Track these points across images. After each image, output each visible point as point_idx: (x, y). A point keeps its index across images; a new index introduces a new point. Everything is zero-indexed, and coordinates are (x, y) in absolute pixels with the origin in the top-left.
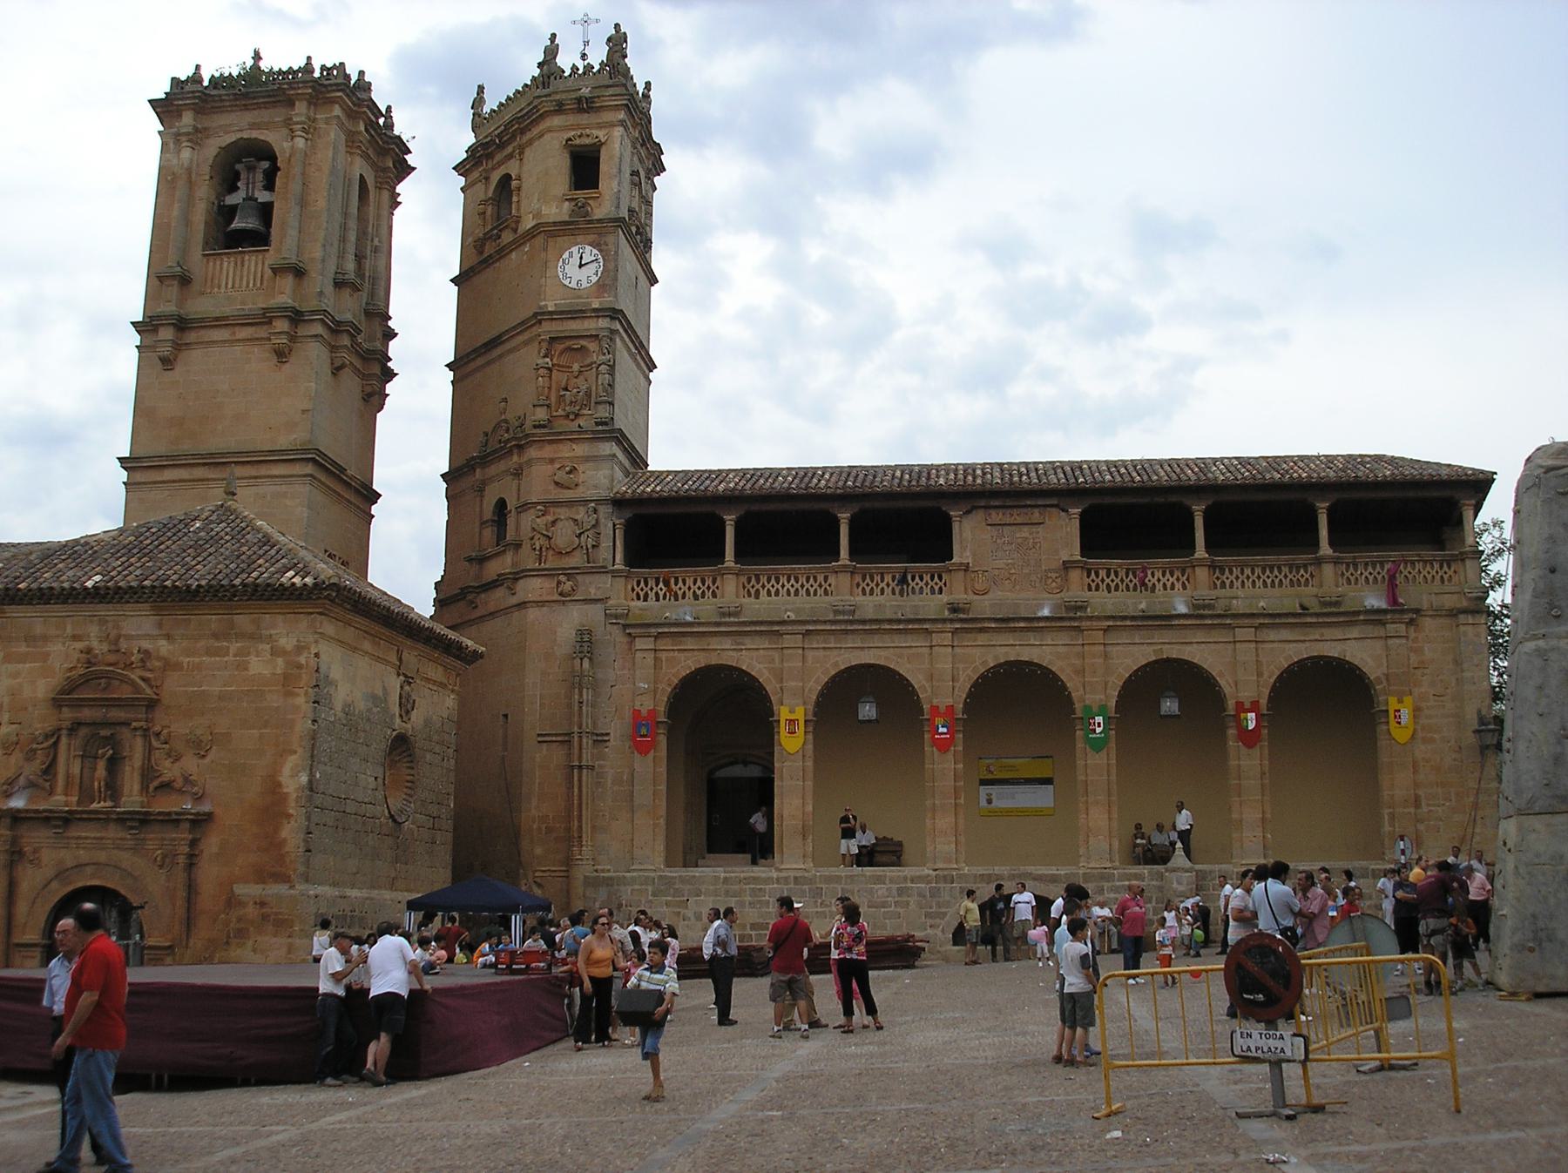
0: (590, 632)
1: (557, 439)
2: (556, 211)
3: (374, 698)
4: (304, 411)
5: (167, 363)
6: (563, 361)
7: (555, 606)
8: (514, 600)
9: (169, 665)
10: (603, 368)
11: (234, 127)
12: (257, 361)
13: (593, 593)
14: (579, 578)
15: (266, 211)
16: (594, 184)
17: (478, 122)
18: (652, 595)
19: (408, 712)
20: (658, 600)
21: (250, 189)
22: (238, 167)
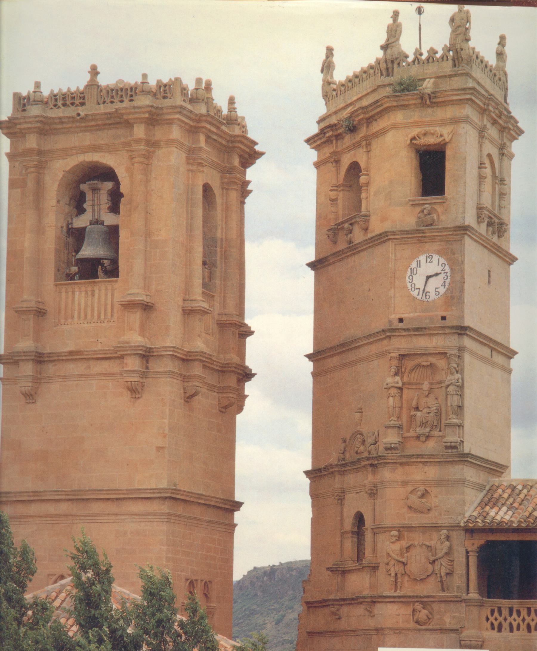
1: (406, 461)
5: (30, 397)
6: (415, 376)
8: (371, 623)
10: (451, 389)
13: (448, 621)
14: (435, 606)
15: (112, 234)
17: (330, 91)
18: (506, 625)
20: (511, 630)
22: (84, 187)
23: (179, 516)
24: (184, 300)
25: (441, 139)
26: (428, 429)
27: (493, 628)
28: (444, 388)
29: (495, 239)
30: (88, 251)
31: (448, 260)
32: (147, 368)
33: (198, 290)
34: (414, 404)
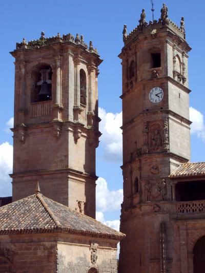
3: (81, 258)
5: (23, 142)
9: (15, 253)
11: (37, 59)
18: (185, 210)
19: (94, 261)
23: (141, 265)
29: (181, 83)
30: (41, 92)
31: (162, 89)
33: (79, 104)
34: (152, 138)
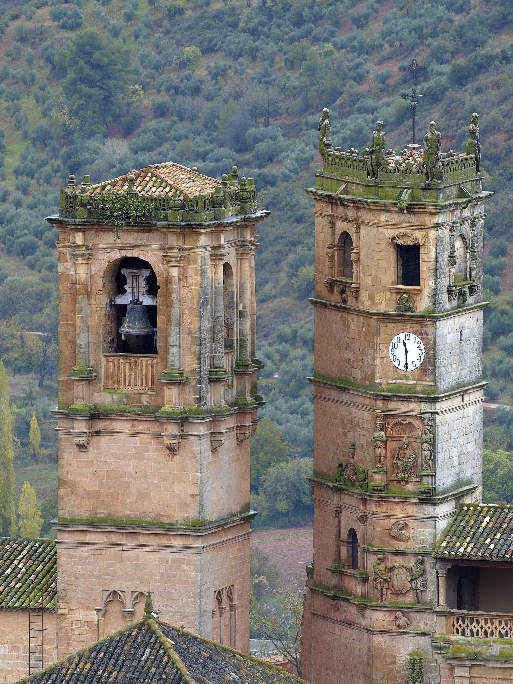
0: (421, 661)
2: (385, 304)
4: (193, 496)
6: (396, 432)
7: (394, 636)
12: (153, 453)
14: (412, 615)
15: (151, 313)
16: (417, 283)
18: (468, 631)
20: (472, 635)
21: (135, 294)
24: (210, 371)
25: (416, 242)
26: (407, 476)
27: (458, 632)
28: (419, 444)
32: (182, 431)
